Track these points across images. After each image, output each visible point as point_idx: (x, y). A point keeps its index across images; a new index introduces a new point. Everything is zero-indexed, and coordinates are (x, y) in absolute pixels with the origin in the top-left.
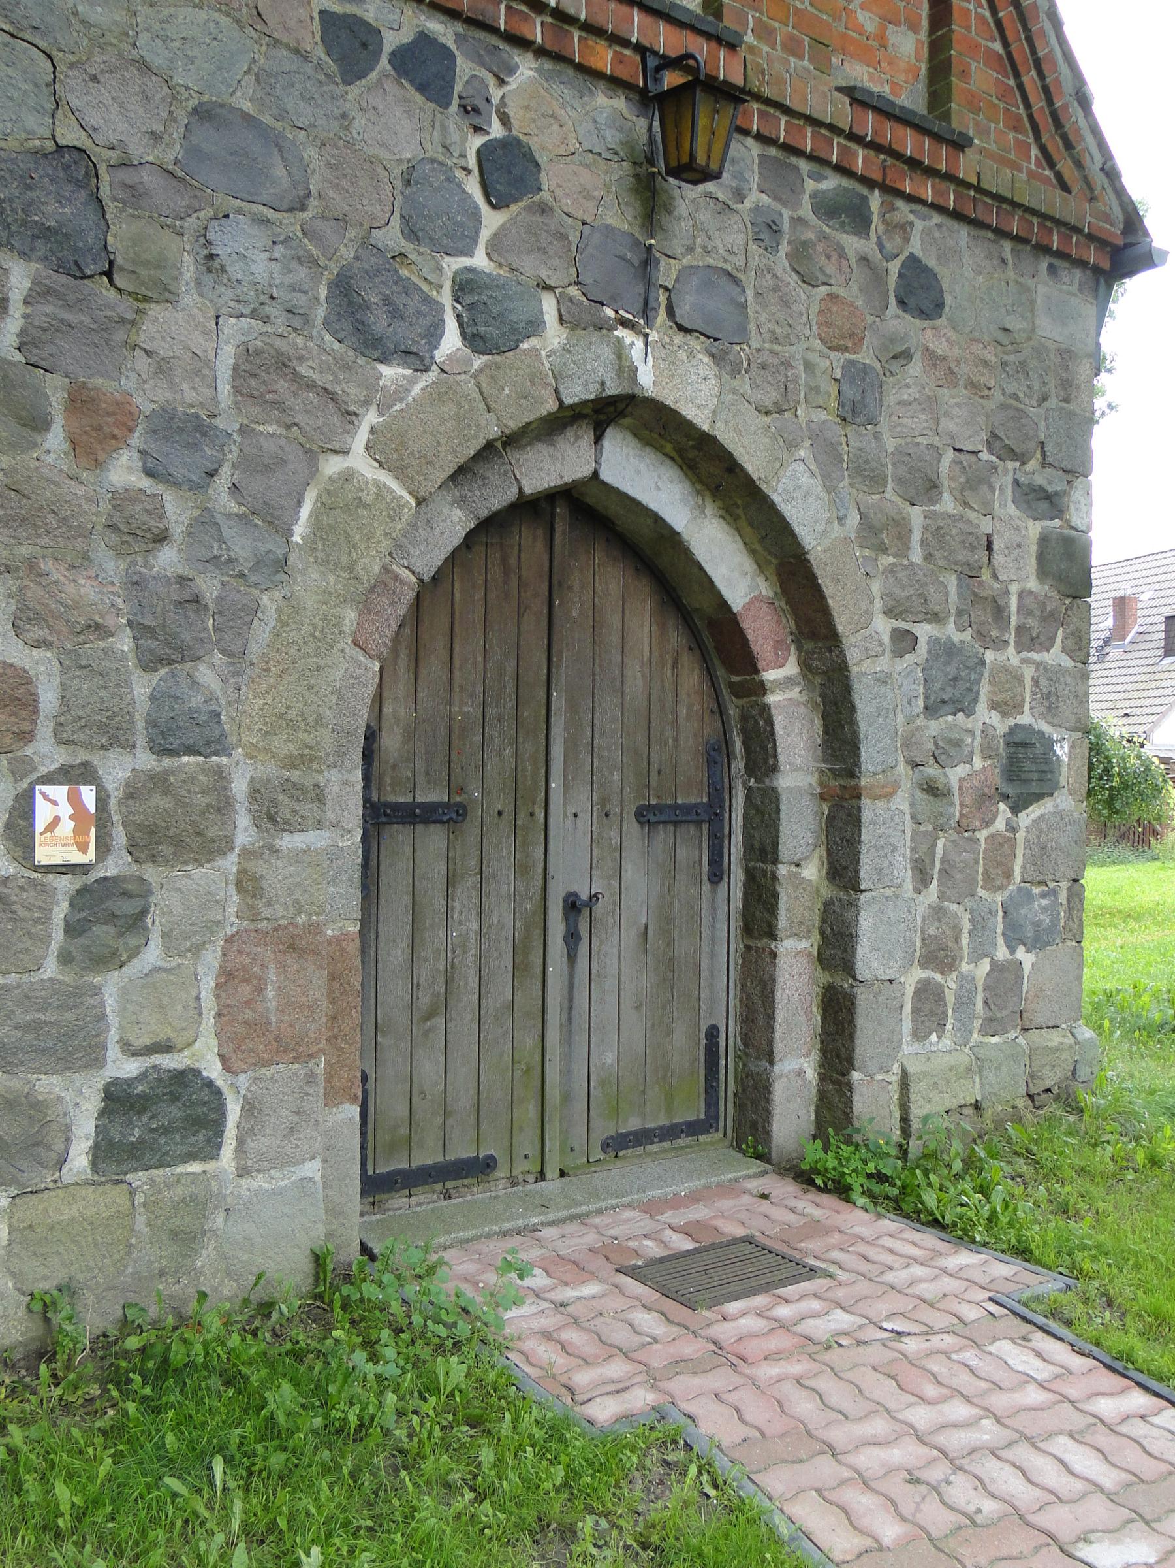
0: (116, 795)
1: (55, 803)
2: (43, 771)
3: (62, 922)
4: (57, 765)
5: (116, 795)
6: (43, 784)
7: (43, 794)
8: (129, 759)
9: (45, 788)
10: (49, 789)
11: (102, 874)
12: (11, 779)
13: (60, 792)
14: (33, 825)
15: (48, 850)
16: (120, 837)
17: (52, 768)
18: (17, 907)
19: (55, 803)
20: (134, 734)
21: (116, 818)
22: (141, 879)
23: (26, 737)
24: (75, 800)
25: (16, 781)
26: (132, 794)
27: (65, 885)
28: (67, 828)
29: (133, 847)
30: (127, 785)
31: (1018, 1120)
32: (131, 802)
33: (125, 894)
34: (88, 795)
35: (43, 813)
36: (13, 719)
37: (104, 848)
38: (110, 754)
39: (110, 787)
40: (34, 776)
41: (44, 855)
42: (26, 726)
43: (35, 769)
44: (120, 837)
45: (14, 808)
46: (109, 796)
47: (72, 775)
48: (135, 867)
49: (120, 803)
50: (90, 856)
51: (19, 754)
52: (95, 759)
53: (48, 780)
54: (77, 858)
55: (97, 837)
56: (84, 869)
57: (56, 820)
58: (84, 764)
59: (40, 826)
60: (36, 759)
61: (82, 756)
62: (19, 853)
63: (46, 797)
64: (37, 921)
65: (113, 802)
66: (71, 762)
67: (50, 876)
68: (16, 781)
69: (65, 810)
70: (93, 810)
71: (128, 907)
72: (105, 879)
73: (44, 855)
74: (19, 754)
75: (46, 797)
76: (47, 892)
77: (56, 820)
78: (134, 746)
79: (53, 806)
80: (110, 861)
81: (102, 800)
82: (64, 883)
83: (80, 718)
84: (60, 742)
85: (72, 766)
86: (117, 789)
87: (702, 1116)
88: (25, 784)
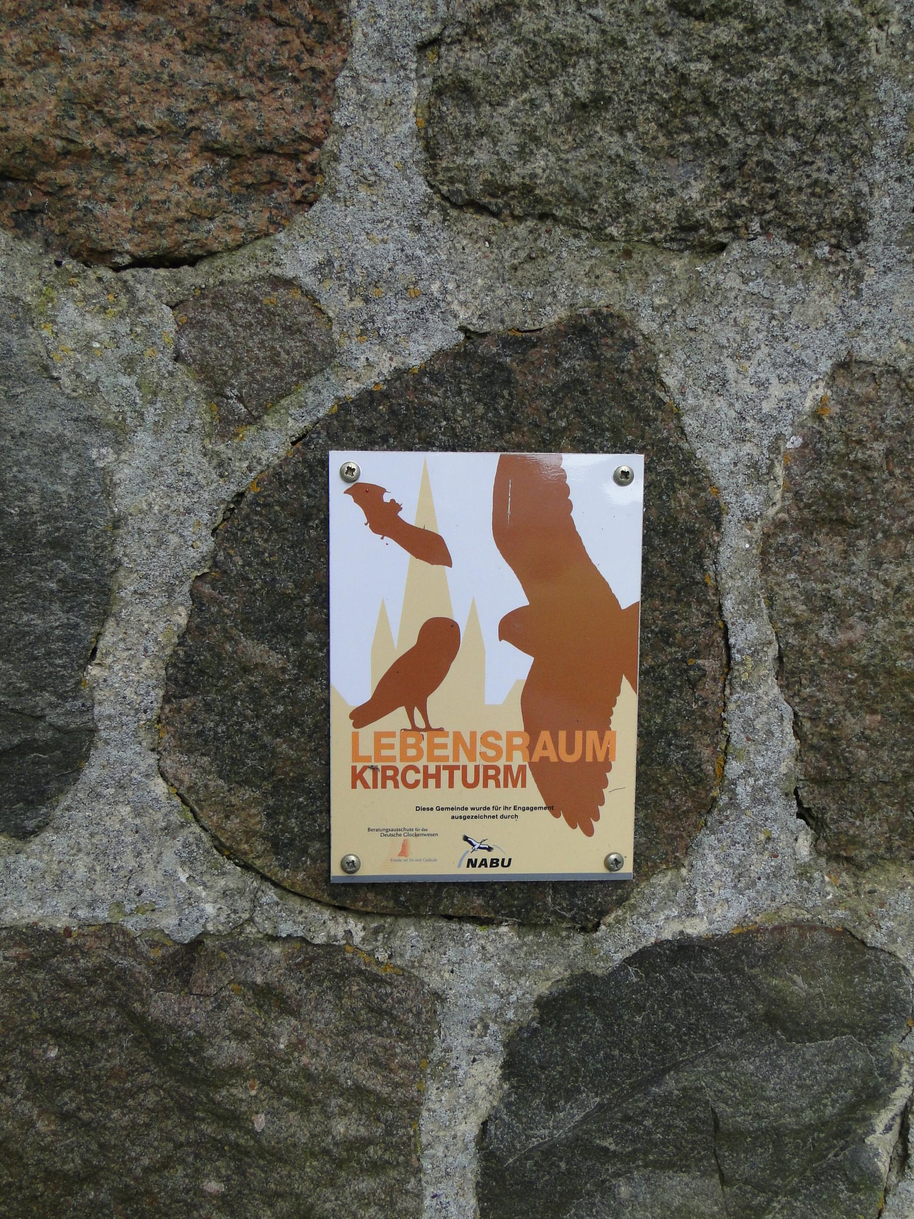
0: (749, 506)
1: (428, 547)
2: (369, 365)
3: (467, 1162)
4: (441, 337)
5: (749, 506)
6: (371, 440)
7: (369, 497)
8: (823, 301)
9: (380, 467)
10: (392, 470)
11: (665, 925)
12: (197, 412)
13: (453, 487)
14: (316, 666)
15: (394, 804)
16: (763, 735)
17: (417, 351)
18: (244, 1092)
19: (428, 547)
20: (853, 156)
21: (749, 632)
22: (849, 943)
23: (282, 172)
24: (535, 533)
25: (226, 426)
26: (832, 501)
27: (481, 980)
28: (493, 679)
29: (826, 793)
30: (813, 454)
31: (88, 198)
32: (828, 547)
33: (784, 1024)
34: (606, 502)
35: (369, 602)
36: (209, 72)
37: (680, 796)
38: (725, 275)
39: (720, 460)
40: (322, 397)
41: (375, 828)
42: (279, 114)
43: (325, 358)
44: (763, 735)
45: (216, 572)
46: (714, 514)
47: (516, 394)
48: (829, 884)
49: (769, 552)
50: (612, 837)
51: (241, 270)
52: (645, 300)
53: (400, 417)
54: (543, 847)
55: (647, 737)
56: (577, 903)
57: (438, 644)
58: (592, 331)
59: (352, 677)
60: (337, 301)
61: (575, 281)
62: (250, 813)
63: (382, 515)
64: (347, 1157)
65: (736, 545)
66: (518, 316)
67: (411, 937)
68: (226, 426)
69: (484, 587)
70: (626, 584)
71: (783, 1085)
72: (684, 950)
73: (375, 828)
74: (241, 270)
75: (382, 515)
76: (395, 1015)
77: (438, 644)
78: (854, 229)
79: (422, 558)
80: (710, 859)
81: (676, 535)
82: (475, 970)
83: (567, 51)
84: (458, 200)
85: (521, 342)
86: (758, 474)
87: (635, 462)
88: (271, 443)
